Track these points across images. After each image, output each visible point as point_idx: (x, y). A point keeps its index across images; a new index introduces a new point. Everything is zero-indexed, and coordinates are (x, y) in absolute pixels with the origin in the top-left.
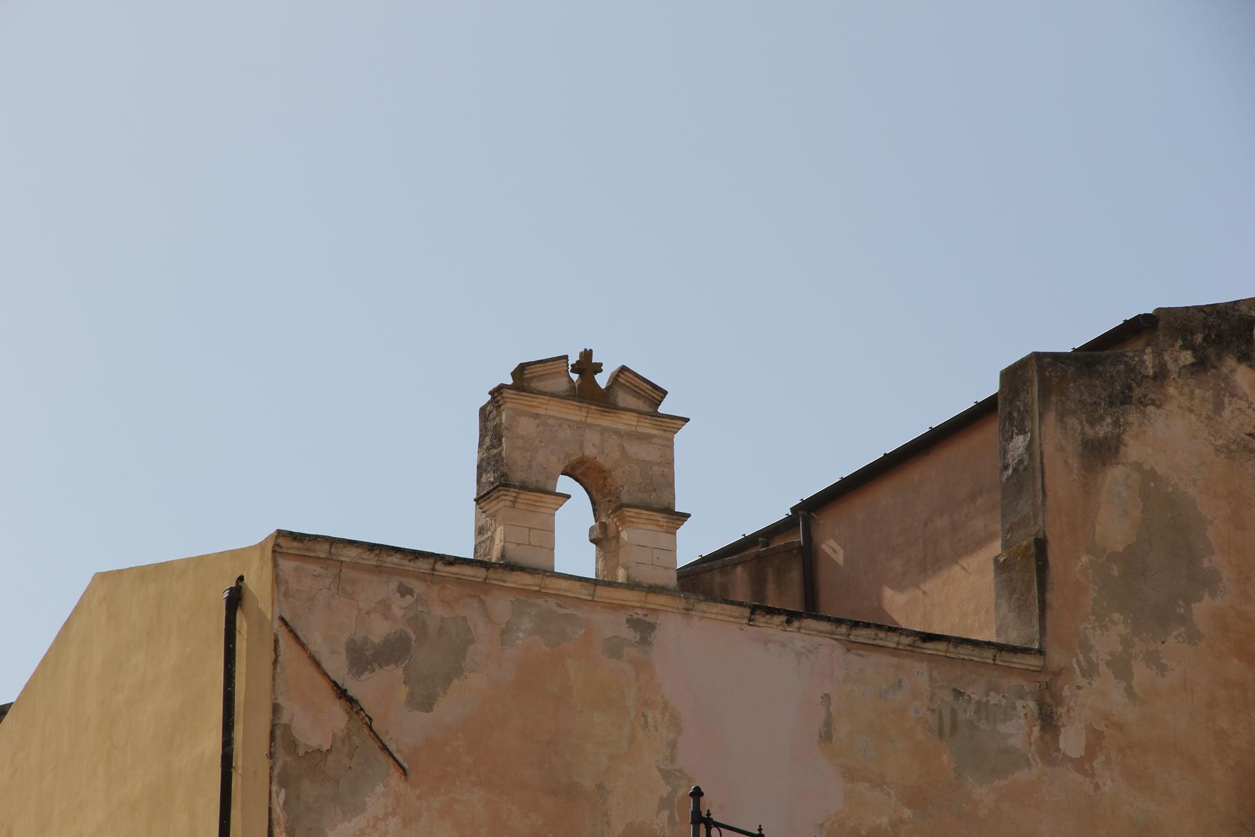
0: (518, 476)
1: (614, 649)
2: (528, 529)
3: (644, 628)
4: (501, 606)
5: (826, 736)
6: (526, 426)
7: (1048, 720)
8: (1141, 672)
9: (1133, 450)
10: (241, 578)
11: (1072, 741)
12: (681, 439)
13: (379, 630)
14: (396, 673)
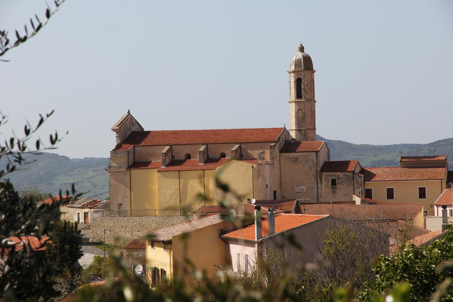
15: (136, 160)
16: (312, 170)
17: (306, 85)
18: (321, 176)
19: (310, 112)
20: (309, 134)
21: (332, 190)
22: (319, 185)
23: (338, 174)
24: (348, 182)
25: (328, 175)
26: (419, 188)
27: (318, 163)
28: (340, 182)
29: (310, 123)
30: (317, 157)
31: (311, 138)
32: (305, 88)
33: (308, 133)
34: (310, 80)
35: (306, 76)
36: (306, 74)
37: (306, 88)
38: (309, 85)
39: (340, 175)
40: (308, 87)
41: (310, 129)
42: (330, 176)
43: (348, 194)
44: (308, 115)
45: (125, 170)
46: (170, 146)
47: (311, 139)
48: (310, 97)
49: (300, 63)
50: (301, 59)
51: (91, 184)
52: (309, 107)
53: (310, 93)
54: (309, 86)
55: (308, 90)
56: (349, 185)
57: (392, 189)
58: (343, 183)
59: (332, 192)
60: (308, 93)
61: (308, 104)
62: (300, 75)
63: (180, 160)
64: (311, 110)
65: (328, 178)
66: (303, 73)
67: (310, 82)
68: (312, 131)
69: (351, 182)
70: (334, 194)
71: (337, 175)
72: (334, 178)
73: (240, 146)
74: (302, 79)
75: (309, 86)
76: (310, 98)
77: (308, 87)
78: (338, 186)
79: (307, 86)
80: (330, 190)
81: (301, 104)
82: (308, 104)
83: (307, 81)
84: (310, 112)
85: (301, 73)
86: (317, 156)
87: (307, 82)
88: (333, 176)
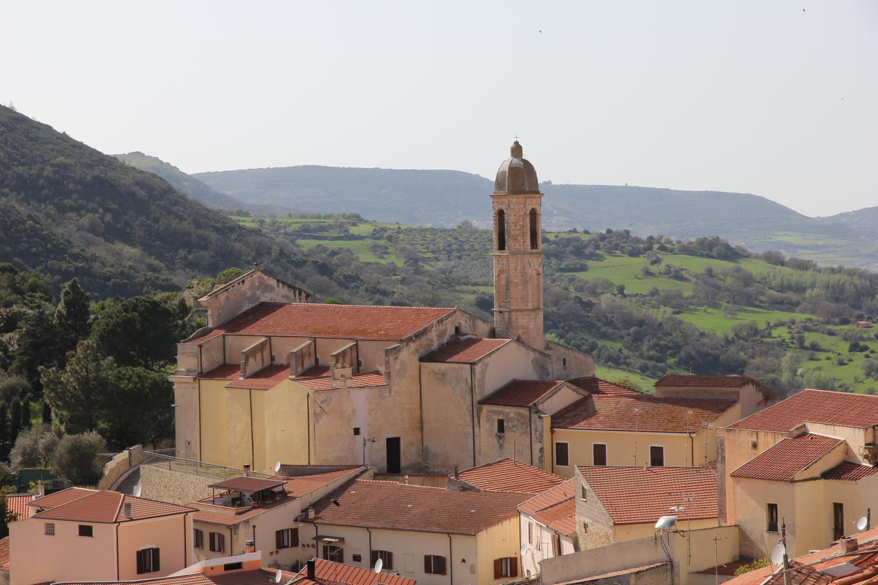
0: (336, 378)
1: (346, 395)
2: (468, 366)
3: (349, 392)
4: (335, 393)
5: (368, 399)
6: (337, 372)
7: (390, 392)
8: (400, 384)
9: (400, 357)
10: (517, 150)
11: (393, 394)
12: (614, 229)
13: (324, 399)
14: (325, 403)
15: (227, 361)
16: (465, 400)
17: (513, 223)
18: (480, 411)
19: (522, 276)
20: (519, 320)
21: (499, 441)
22: (476, 428)
23: (507, 410)
24: (523, 428)
25: (493, 412)
26: (652, 448)
27: (473, 385)
28: (510, 427)
29: (522, 298)
30: (473, 375)
31: (523, 328)
32: (510, 230)
33: (517, 319)
34: (522, 213)
35: (512, 206)
36: (512, 202)
37: (513, 230)
38: (521, 223)
39: (509, 412)
40: (518, 227)
41: (521, 311)
42: (495, 412)
43: (522, 452)
44: (516, 283)
45: (191, 381)
46: (266, 339)
47: (524, 330)
48: (522, 247)
49: (504, 179)
50: (506, 172)
51: (674, 310)
52: (519, 268)
53: (521, 239)
54: (520, 226)
55: (518, 232)
56: (525, 433)
57: (603, 447)
58: (515, 428)
59: (498, 446)
60: (516, 239)
61: (517, 260)
62: (503, 203)
63: (282, 365)
64: (524, 273)
65: (491, 416)
66: (506, 201)
67: (521, 218)
68: (526, 315)
69: (526, 428)
70: (501, 450)
71: (506, 412)
72: (501, 417)
73: (357, 345)
74: (505, 212)
75: (520, 226)
76: (522, 249)
77: (518, 227)
78: (507, 434)
79: (516, 226)
80: (495, 441)
81: (503, 260)
82: (517, 260)
83: (515, 215)
84: (522, 276)
85: (503, 200)
86: (472, 372)
87: (516, 217)
88: (499, 413)
